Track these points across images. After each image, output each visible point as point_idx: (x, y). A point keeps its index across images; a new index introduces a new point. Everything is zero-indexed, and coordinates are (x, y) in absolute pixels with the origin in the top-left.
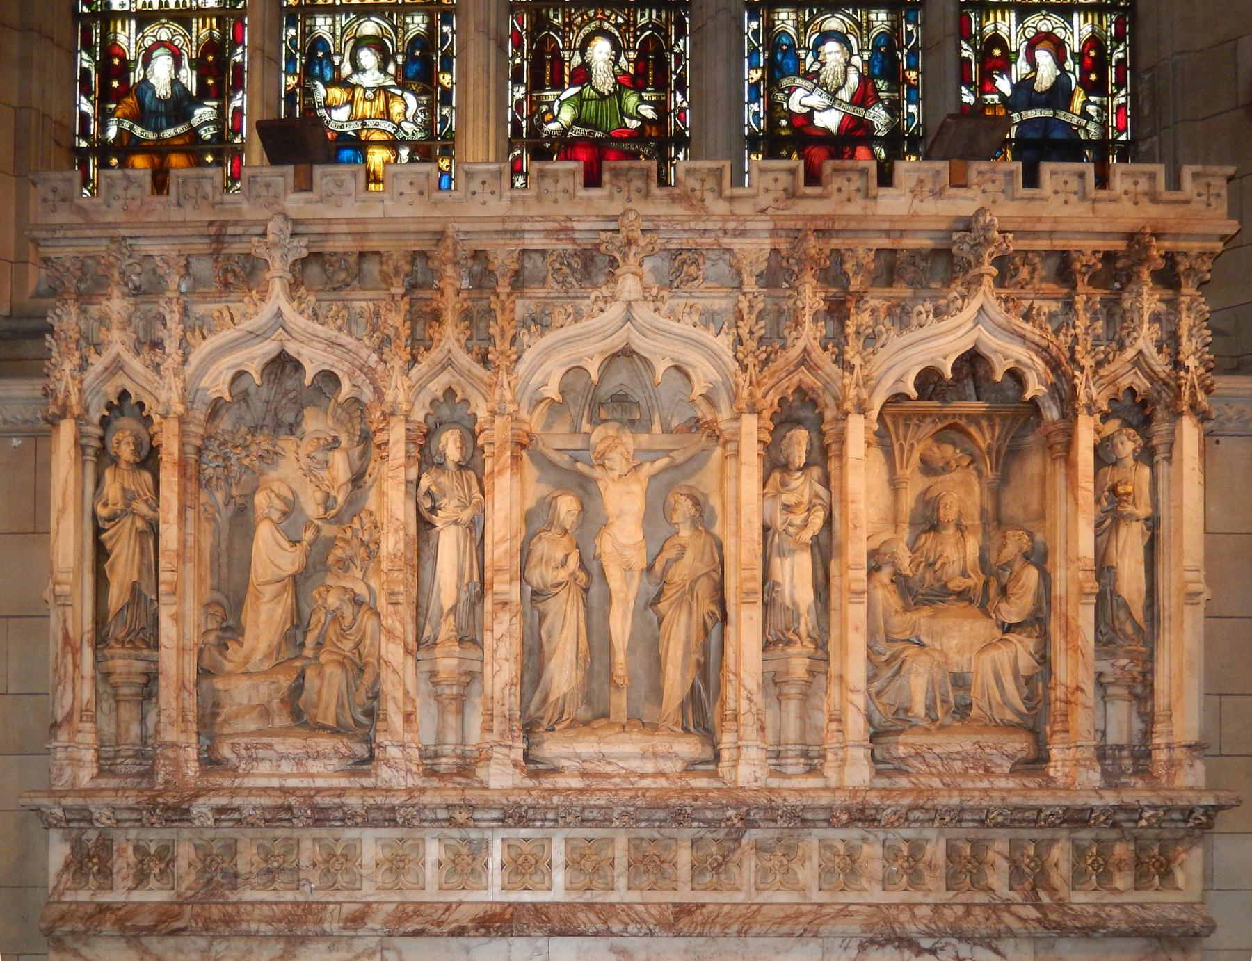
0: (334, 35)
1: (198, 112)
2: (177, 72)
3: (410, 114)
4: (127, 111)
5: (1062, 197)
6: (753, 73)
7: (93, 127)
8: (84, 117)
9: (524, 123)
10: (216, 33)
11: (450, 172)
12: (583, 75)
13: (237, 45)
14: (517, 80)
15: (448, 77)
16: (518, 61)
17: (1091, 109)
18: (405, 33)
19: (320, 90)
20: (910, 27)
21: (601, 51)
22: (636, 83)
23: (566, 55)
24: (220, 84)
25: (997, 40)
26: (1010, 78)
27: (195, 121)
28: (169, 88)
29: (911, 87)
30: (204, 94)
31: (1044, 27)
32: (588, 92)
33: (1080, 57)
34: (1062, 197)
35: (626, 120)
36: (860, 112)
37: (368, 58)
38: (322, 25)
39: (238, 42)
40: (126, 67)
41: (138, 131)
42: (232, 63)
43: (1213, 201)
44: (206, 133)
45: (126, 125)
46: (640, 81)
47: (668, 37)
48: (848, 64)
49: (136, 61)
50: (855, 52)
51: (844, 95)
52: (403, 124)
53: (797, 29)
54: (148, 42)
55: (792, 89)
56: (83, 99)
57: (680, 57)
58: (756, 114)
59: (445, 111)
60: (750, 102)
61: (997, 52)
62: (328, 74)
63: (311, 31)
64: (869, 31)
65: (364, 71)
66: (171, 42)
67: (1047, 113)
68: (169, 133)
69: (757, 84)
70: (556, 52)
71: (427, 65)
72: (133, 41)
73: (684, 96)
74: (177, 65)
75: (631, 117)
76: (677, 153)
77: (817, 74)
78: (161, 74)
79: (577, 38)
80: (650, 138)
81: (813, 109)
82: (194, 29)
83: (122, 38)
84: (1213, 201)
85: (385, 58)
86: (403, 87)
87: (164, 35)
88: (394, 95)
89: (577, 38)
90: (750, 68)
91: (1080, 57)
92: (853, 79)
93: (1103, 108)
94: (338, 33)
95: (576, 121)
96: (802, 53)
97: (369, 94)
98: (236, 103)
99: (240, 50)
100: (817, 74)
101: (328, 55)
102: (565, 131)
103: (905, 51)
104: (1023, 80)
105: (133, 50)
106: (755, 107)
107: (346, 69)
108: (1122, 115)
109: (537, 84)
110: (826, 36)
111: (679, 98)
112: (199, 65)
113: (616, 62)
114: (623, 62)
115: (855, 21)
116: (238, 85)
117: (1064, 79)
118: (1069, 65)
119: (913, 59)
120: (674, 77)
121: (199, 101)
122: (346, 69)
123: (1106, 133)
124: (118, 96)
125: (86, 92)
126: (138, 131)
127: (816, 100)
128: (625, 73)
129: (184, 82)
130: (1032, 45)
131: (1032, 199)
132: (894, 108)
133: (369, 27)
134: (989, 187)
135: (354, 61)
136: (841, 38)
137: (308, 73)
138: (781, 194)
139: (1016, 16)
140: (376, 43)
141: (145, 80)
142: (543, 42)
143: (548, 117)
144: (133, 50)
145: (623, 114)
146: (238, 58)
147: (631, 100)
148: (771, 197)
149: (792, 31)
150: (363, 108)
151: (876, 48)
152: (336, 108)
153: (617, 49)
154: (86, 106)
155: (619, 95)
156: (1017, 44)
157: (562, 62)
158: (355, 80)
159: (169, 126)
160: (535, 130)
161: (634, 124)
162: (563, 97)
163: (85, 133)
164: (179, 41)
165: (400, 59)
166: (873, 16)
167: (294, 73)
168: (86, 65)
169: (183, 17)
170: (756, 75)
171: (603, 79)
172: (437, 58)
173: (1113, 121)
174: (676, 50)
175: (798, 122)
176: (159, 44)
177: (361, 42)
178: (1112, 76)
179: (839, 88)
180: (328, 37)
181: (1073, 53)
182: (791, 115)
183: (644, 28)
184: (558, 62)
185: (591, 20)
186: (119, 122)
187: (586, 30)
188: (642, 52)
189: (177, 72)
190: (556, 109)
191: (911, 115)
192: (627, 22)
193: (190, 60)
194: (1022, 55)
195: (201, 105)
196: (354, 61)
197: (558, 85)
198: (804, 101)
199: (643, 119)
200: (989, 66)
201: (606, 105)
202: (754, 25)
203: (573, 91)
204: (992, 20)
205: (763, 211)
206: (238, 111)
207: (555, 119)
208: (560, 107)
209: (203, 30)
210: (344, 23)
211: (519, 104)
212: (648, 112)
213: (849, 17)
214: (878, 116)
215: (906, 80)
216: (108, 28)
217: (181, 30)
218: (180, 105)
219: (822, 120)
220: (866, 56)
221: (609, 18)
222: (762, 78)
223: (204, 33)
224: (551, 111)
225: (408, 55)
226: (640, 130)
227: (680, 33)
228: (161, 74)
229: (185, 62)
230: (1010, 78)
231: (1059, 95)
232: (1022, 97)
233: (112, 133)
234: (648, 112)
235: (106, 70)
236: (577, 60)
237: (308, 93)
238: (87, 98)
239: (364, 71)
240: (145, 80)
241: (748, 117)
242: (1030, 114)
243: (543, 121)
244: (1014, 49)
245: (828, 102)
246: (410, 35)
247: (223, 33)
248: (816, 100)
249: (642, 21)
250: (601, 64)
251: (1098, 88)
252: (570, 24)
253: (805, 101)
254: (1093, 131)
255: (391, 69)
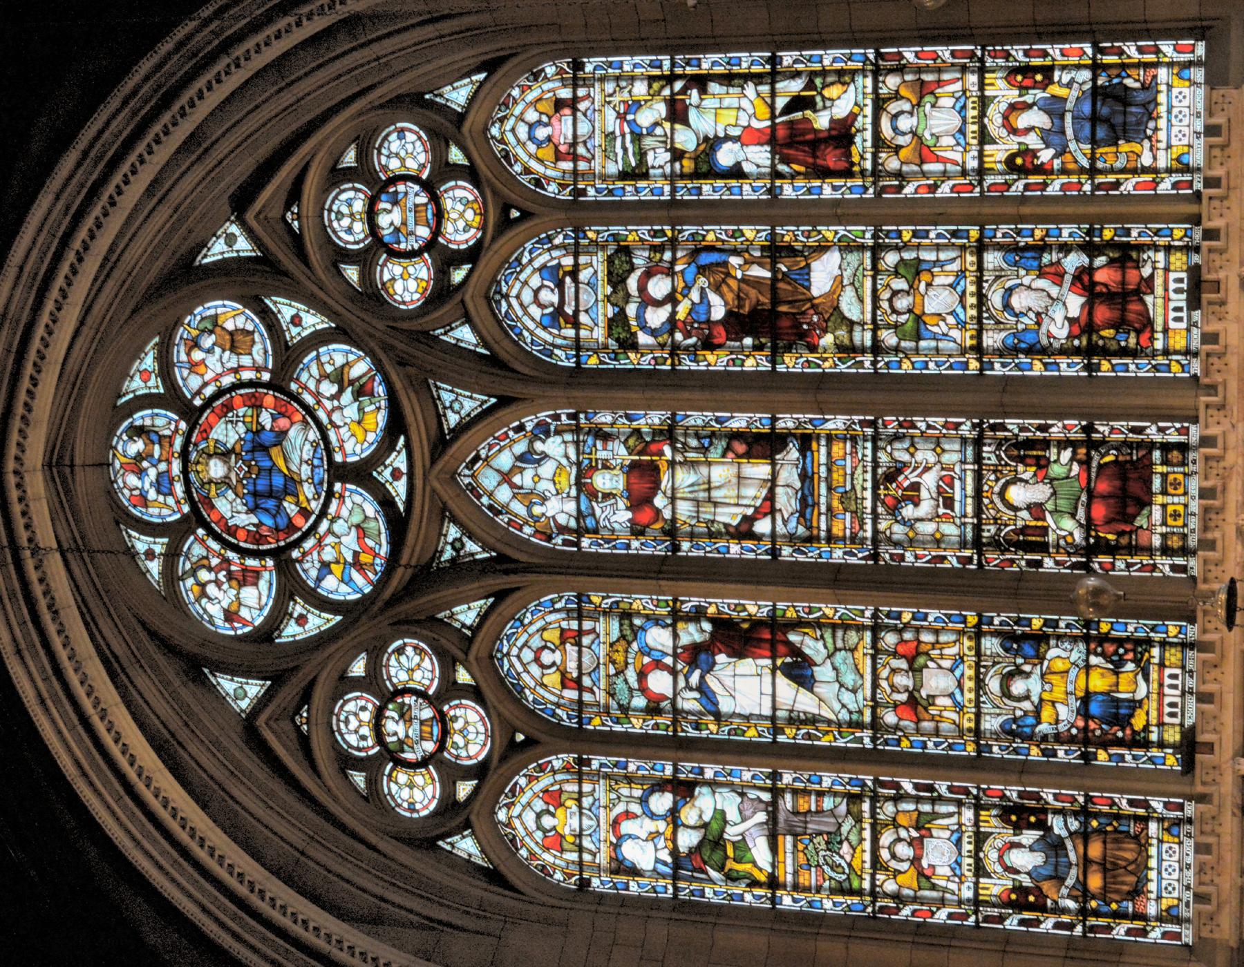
0: (999, 715)
1: (1056, 831)
2: (1024, 847)
3: (1064, 654)
4: (1054, 890)
5: (1225, 211)
6: (1035, 368)
7: (1065, 919)
8: (1058, 926)
9: (1074, 560)
10: (994, 812)
11: (1112, 623)
12: (1036, 509)
13: (1004, 795)
14: (1039, 564)
15: (1034, 622)
16: (1023, 563)
17: (1066, 78)
18: (999, 656)
19: (1043, 728)
20: (999, 235)
21: (1017, 494)
22: (1042, 464)
23: (1020, 524)
24: (1033, 811)
25: (1010, 161)
26: (1039, 150)
27: (1064, 833)
28: (1036, 854)
29: (1047, 235)
30: (1042, 825)
31: (999, 120)
32: (1050, 506)
33: (1023, 89)
34: (1225, 211)
35: (1072, 474)
36: (1068, 278)
37: (1018, 687)
38: (990, 724)
39: (1003, 797)
40: (1019, 889)
41: (1070, 882)
42: (1018, 800)
43: (1227, 100)
44: (1074, 825)
45: (1064, 891)
46: (1043, 462)
47: (1006, 439)
48: (1029, 287)
49: (1014, 880)
50: (1019, 281)
51: (1054, 291)
52: (1072, 660)
53: (1001, 330)
54: (999, 869)
55: (1049, 335)
56: (1043, 926)
57: (1023, 429)
58: (1069, 365)
59: (1062, 624)
60: (1059, 370)
61: (1019, 161)
62: (1030, 721)
63: (996, 733)
64: (1002, 270)
65: (1028, 690)
66: (999, 850)
67: (1068, 118)
68: (1073, 857)
69: (1045, 365)
70: (1019, 532)
71: (1025, 637)
72: (998, 882)
73: (1053, 425)
74: (1019, 845)
75: (1070, 470)
76: (1098, 432)
77: (1038, 314)
78: (1025, 860)
79: (1007, 514)
80: (1088, 454)
81: (1066, 318)
82: (990, 830)
83: (996, 890)
84: (1227, 100)
85: (1018, 672)
86: (1041, 658)
87: (994, 855)
88: (1048, 667)
89: (1007, 514)
90: (1031, 370)
91: (1023, 89)
92: (1042, 283)
93: (1064, 68)
94: (998, 711)
95: (1073, 516)
96: (1021, 327)
97: (1047, 687)
98: (1050, 799)
99: (1008, 793)
100: (1038, 314)
101: (1015, 720)
102: (1081, 525)
103: (1019, 239)
104: (1042, 138)
105: (1004, 882)
106: (1063, 366)
107: (1027, 705)
108: (1070, 53)
109: (1043, 548)
110: (1007, 306)
111: (1054, 429)
112: (1018, 828)
113: (1026, 482)
114: (1026, 476)
115: (994, 281)
116: (1037, 797)
117: (1041, 103)
118: (1029, 99)
119: (1024, 233)
120: (1038, 433)
121: (1049, 829)
122: (1027, 705)
123: (1085, 67)
124: (1041, 895)
125: (1037, 922)
126: (1070, 882)
127: (1059, 315)
128: (1035, 475)
129: (1031, 841)
130: (1014, 131)
131: (1227, 235)
132: (1065, 248)
133: (994, 684)
134: (1218, 264)
135: (1019, 699)
136: (1009, 292)
137: (1029, 738)
138: (1222, 413)
139: (989, 143)
140: (1007, 678)
141: (1028, 873)
142: (1010, 543)
143: (1069, 540)
144: (1004, 882)
145: (1067, 478)
146: (1015, 795)
147: (1056, 470)
148: (1223, 420)
149: (1003, 334)
150: (1058, 694)
151: (1016, 264)
152: (1057, 715)
153: (1016, 480)
154: (1048, 925)
155: (1052, 480)
156: (1011, 144)
157: (1026, 527)
158: (1035, 699)
159: (1067, 856)
160: (1078, 550)
161: (1076, 468)
162: (1054, 527)
163: (1071, 927)
164: (999, 843)
165: (1020, 661)
166: (991, 266)
167: (1029, 749)
168: (1015, 922)
169: (980, 839)
170: (1038, 365)
171: (1039, 493)
172: (1019, 630)
173: (1074, 60)
174: (1016, 431)
175: (1077, 331)
176: (1000, 859)
177: (1006, 693)
178: (1037, 62)
179: (1049, 295)
180: (1001, 719)
181: (1020, 96)
182: (1070, 337)
183: (999, 458)
184: (1024, 530)
185: (992, 502)
186: (1062, 897)
187: (1000, 505)
188: (1021, 460)
189: (1024, 847)
190: (1063, 533)
191: (1070, 235)
192: (995, 472)
193: (1015, 835)
194: (1021, 139)
195: (1051, 829)
196: (1019, 699)
197: (1044, 531)
198: (1059, 325)
199: (1072, 459)
200: (1030, 166)
201: (1060, 491)
202: (997, 366)
203: (1048, 516)
204: (992, 165)
205: (1233, 426)
206: (1057, 797)
207: (1071, 534)
208: (1061, 529)
209: (991, 822)
210: (989, 706)
211: (1057, 563)
212: (1066, 455)
213: (990, 286)
214: (1074, 261)
215: (1042, 239)
216: (987, 902)
217: (990, 841)
218: (1053, 847)
219: (1074, 311)
220: (1022, 272)
221: (991, 487)
222: (1040, 360)
223: (994, 822)
224: (1064, 537)
225: (1017, 653)
226: (1080, 463)
227: (1003, 427)
228: (1025, 860)
229: (1016, 839)
230: (1039, 150)
231: (1055, 108)
232: (1056, 139)
233: (1071, 904)
234: (1066, 455)
235: (1019, 906)
236: (1024, 514)
237: (1045, 738)
238: (1041, 922)
239: (1028, 690)
240: (1028, 873)
241: (1071, 373)
242: (1069, 132)
243: (1072, 545)
244: (1016, 147)
245: (1061, 305)
246: (1001, 651)
247: (995, 806)
248: (1059, 315)
249: (994, 460)
250: (1028, 494)
251: (1048, 71)
252: (995, 519)
253: (1059, 324)
254: (1085, 75)
255: (1027, 668)
